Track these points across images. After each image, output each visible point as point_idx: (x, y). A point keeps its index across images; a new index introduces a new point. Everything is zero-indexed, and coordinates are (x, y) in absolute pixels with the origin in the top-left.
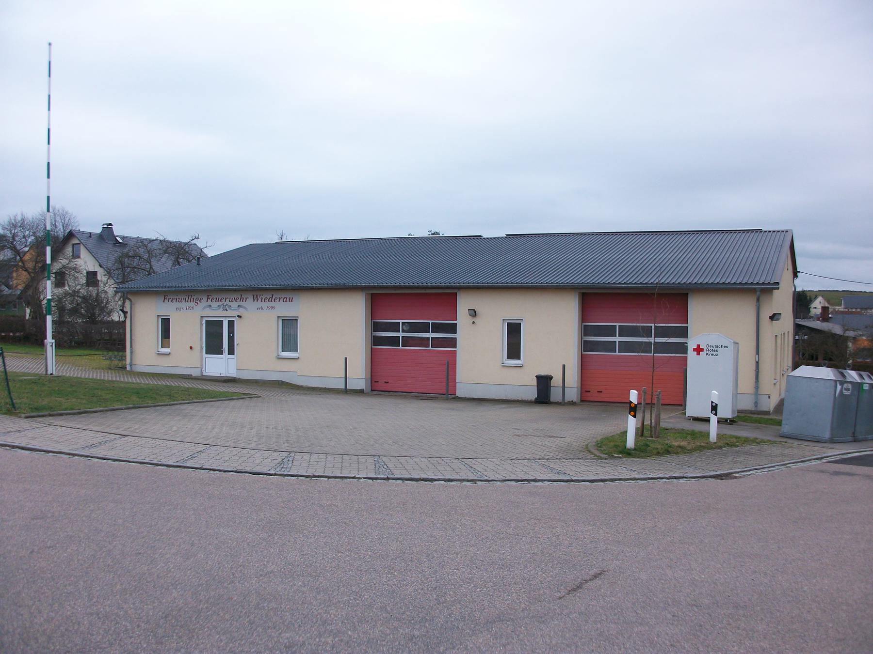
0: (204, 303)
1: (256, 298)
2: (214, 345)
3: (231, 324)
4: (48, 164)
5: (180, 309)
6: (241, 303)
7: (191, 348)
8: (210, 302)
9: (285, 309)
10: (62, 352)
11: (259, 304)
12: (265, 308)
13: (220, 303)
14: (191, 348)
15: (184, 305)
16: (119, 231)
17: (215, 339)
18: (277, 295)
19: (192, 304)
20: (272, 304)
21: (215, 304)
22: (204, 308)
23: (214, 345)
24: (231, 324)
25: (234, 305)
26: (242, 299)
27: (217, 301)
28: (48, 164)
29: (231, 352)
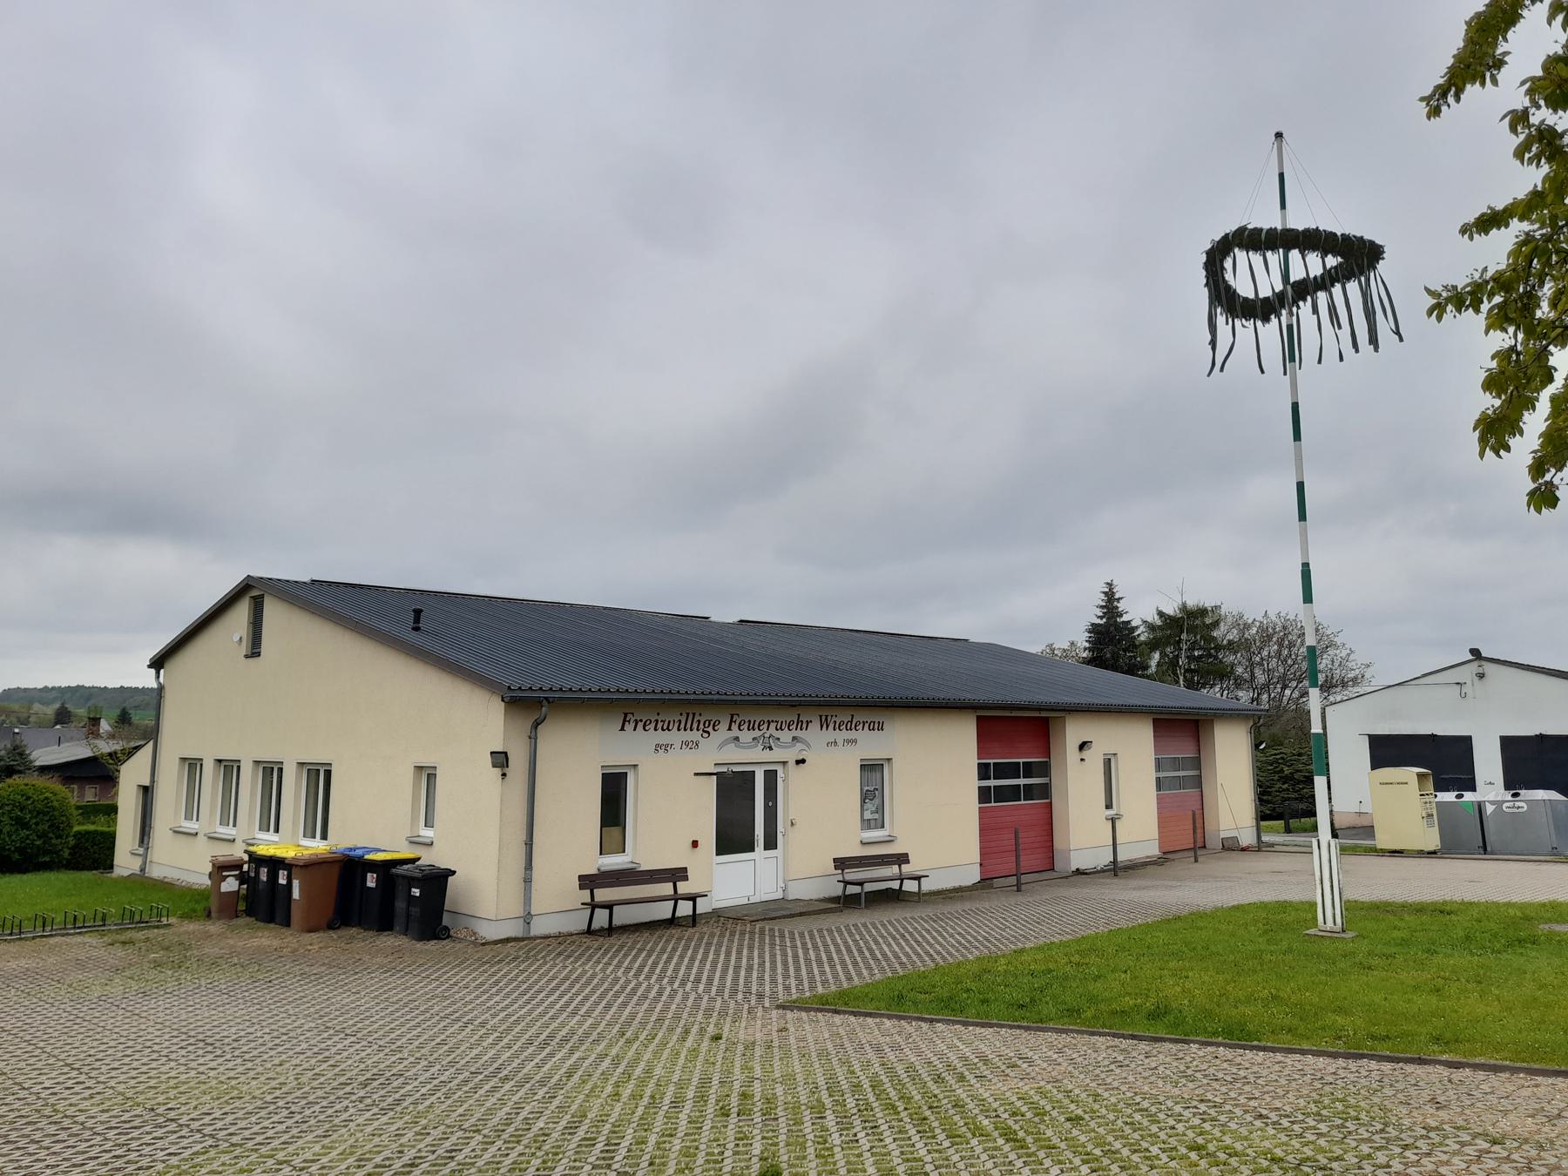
0: (722, 733)
1: (824, 724)
2: (733, 837)
3: (771, 777)
4: (1295, 408)
5: (666, 747)
6: (798, 733)
7: (695, 844)
8: (735, 732)
9: (870, 744)
10: (335, 872)
11: (830, 735)
12: (840, 742)
13: (757, 733)
14: (695, 844)
15: (675, 737)
16: (1141, 611)
17: (739, 821)
18: (860, 716)
19: (695, 735)
20: (852, 735)
21: (746, 736)
22: (721, 746)
23: (733, 837)
24: (771, 777)
25: (785, 736)
26: (801, 724)
27: (751, 728)
28: (1295, 408)
29: (771, 843)
